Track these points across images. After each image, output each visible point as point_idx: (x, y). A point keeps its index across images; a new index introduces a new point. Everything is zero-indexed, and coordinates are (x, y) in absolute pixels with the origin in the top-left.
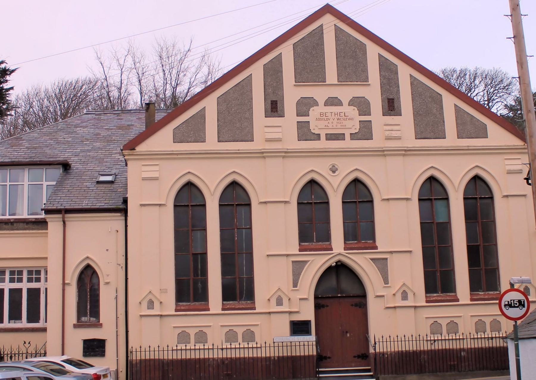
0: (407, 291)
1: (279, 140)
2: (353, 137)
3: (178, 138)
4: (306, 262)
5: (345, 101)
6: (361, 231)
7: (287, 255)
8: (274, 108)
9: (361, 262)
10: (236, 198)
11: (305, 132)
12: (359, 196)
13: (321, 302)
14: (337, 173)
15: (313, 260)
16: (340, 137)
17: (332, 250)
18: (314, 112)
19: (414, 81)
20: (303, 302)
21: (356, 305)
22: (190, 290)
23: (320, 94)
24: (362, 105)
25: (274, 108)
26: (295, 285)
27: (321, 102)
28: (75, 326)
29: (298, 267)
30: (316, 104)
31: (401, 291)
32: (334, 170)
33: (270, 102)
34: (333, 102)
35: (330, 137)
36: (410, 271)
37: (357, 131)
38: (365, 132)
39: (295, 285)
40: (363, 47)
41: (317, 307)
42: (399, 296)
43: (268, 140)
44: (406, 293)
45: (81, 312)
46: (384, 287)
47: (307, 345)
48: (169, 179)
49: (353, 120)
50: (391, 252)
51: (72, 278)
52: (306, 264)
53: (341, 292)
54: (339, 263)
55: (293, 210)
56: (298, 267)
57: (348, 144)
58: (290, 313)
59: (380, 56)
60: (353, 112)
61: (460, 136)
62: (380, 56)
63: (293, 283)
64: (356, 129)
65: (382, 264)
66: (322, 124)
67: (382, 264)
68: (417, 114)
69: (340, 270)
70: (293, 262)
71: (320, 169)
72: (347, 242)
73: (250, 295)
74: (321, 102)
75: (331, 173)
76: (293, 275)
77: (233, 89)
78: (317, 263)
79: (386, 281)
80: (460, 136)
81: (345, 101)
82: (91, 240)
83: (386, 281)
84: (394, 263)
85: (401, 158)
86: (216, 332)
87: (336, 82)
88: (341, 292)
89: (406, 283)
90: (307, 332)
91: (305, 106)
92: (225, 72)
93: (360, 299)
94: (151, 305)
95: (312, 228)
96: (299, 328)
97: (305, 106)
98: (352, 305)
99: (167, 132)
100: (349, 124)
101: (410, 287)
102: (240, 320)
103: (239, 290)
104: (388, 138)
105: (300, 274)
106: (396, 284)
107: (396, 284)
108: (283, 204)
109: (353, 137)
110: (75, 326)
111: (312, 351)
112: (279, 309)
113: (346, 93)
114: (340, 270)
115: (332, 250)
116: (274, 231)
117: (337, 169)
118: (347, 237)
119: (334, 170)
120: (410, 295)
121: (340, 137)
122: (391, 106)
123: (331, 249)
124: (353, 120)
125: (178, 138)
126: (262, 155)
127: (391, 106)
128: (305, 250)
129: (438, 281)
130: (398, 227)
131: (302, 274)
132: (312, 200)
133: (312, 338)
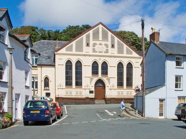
1: (88, 52)
2: (104, 52)
3: (67, 50)
5: (103, 44)
6: (105, 72)
7: (89, 77)
8: (88, 45)
9: (104, 79)
10: (79, 64)
11: (94, 51)
12: (105, 65)
16: (102, 52)
18: (96, 46)
22: (68, 83)
23: (98, 42)
24: (107, 46)
25: (88, 45)
26: (91, 83)
27: (98, 44)
28: (44, 90)
29: (91, 79)
30: (97, 44)
34: (100, 44)
35: (99, 52)
36: (114, 82)
38: (107, 51)
39: (91, 83)
40: (108, 33)
41: (95, 88)
43: (86, 52)
45: (45, 86)
47: (92, 96)
48: (65, 59)
49: (105, 49)
50: (111, 78)
51: (43, 80)
53: (100, 85)
55: (91, 67)
56: (91, 79)
57: (103, 54)
58: (89, 89)
59: (111, 35)
60: (105, 47)
61: (76, 51)
62: (111, 35)
64: (105, 50)
65: (109, 79)
66: (98, 49)
67: (109, 79)
68: (118, 48)
71: (97, 59)
73: (81, 85)
74: (98, 44)
78: (95, 79)
80: (76, 51)
81: (103, 44)
82: (47, 71)
86: (74, 92)
88: (100, 85)
90: (93, 93)
91: (94, 45)
92: (9, 12)
94: (60, 86)
95: (95, 72)
96: (91, 92)
97: (94, 45)
99: (64, 49)
102: (79, 90)
103: (79, 84)
104: (86, 52)
106: (111, 84)
107: (111, 84)
109: (104, 52)
110: (44, 90)
111: (93, 97)
112: (87, 88)
113: (103, 43)
116: (87, 71)
118: (102, 74)
120: (114, 87)
121: (102, 52)
122: (113, 46)
124: (105, 49)
125: (67, 50)
126: (85, 55)
127: (113, 46)
129: (120, 84)
130: (113, 72)
132: (95, 65)
133: (94, 94)
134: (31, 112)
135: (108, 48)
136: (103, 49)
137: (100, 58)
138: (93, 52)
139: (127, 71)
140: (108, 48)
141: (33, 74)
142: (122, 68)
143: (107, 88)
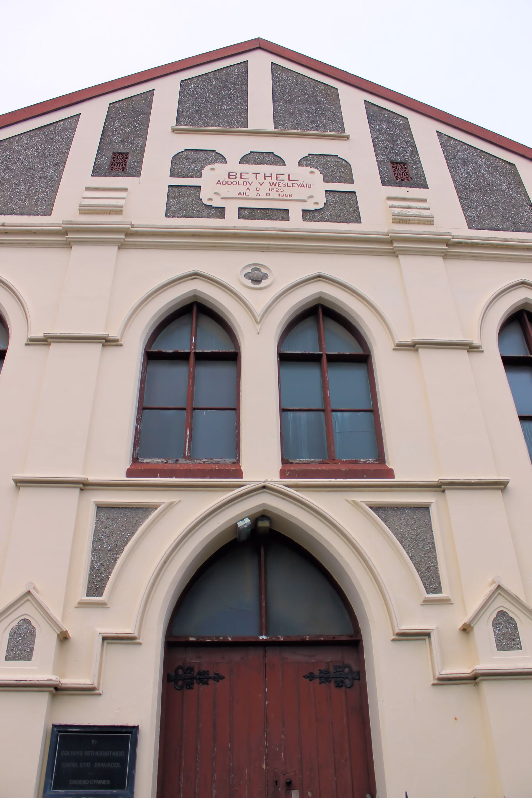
0: (514, 613)
4: (147, 509)
6: (336, 432)
7: (84, 486)
9: (340, 521)
11: (183, 200)
12: (326, 341)
13: (192, 659)
14: (264, 283)
15: (171, 505)
17: (241, 476)
19: (445, 142)
20: (118, 653)
21: (325, 677)
23: (232, 146)
26: (96, 584)
29: (115, 528)
31: (491, 614)
32: (256, 277)
33: (110, 154)
37: (321, 206)
39: (96, 584)
42: (485, 632)
44: (511, 621)
46: (427, 602)
50: (440, 487)
52: (146, 517)
54: (264, 524)
56: (115, 528)
58: (57, 690)
63: (91, 581)
65: (411, 525)
67: (411, 525)
69: (262, 546)
70: (100, 508)
71: (222, 277)
72: (118, 765)
75: (249, 283)
76: (95, 551)
77: (31, 134)
78: (184, 522)
79: (431, 579)
83: (431, 579)
84: (453, 521)
85: (439, 261)
87: (270, 126)
89: (505, 585)
93: (339, 652)
98: (311, 677)
100: (297, 193)
101: (522, 598)
105: (118, 549)
106: (468, 590)
107: (468, 590)
108: (97, 348)
114: (262, 546)
115: (241, 476)
117: (265, 276)
119: (256, 277)
123: (238, 474)
128: (152, 473)
131: (127, 548)
134: (36, 668)
135: (351, 181)
136: (297, 193)
137: (256, 268)
138: (167, 216)
139: (337, 551)
140: (351, 181)
141: (184, 412)
142: (210, 375)
143: (397, 688)
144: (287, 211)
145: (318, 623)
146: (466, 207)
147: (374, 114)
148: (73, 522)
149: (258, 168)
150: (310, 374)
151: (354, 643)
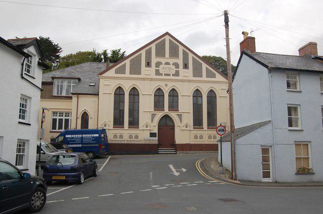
6: (174, 106)
9: (173, 115)
12: (174, 94)
19: (193, 59)
29: (153, 116)
32: (166, 85)
56: (153, 116)
65: (180, 116)
67: (180, 116)
69: (166, 117)
71: (162, 85)
78: (160, 115)
114: (166, 117)
144: (151, 136)
145: (171, 124)
146: (178, 49)
147: (184, 52)
148: (149, 116)
149: (167, 63)
150: (171, 98)
151: (174, 126)
